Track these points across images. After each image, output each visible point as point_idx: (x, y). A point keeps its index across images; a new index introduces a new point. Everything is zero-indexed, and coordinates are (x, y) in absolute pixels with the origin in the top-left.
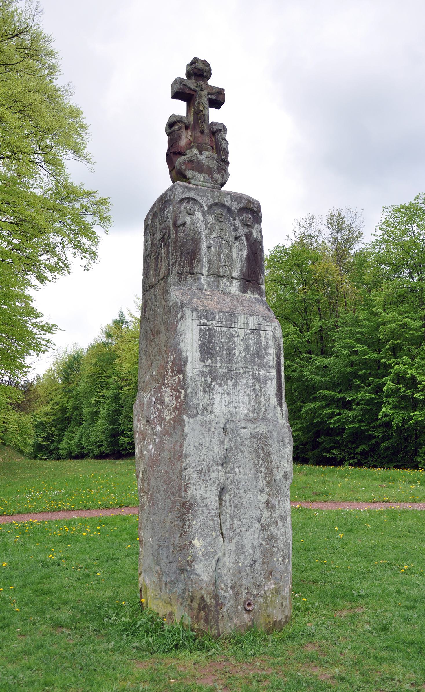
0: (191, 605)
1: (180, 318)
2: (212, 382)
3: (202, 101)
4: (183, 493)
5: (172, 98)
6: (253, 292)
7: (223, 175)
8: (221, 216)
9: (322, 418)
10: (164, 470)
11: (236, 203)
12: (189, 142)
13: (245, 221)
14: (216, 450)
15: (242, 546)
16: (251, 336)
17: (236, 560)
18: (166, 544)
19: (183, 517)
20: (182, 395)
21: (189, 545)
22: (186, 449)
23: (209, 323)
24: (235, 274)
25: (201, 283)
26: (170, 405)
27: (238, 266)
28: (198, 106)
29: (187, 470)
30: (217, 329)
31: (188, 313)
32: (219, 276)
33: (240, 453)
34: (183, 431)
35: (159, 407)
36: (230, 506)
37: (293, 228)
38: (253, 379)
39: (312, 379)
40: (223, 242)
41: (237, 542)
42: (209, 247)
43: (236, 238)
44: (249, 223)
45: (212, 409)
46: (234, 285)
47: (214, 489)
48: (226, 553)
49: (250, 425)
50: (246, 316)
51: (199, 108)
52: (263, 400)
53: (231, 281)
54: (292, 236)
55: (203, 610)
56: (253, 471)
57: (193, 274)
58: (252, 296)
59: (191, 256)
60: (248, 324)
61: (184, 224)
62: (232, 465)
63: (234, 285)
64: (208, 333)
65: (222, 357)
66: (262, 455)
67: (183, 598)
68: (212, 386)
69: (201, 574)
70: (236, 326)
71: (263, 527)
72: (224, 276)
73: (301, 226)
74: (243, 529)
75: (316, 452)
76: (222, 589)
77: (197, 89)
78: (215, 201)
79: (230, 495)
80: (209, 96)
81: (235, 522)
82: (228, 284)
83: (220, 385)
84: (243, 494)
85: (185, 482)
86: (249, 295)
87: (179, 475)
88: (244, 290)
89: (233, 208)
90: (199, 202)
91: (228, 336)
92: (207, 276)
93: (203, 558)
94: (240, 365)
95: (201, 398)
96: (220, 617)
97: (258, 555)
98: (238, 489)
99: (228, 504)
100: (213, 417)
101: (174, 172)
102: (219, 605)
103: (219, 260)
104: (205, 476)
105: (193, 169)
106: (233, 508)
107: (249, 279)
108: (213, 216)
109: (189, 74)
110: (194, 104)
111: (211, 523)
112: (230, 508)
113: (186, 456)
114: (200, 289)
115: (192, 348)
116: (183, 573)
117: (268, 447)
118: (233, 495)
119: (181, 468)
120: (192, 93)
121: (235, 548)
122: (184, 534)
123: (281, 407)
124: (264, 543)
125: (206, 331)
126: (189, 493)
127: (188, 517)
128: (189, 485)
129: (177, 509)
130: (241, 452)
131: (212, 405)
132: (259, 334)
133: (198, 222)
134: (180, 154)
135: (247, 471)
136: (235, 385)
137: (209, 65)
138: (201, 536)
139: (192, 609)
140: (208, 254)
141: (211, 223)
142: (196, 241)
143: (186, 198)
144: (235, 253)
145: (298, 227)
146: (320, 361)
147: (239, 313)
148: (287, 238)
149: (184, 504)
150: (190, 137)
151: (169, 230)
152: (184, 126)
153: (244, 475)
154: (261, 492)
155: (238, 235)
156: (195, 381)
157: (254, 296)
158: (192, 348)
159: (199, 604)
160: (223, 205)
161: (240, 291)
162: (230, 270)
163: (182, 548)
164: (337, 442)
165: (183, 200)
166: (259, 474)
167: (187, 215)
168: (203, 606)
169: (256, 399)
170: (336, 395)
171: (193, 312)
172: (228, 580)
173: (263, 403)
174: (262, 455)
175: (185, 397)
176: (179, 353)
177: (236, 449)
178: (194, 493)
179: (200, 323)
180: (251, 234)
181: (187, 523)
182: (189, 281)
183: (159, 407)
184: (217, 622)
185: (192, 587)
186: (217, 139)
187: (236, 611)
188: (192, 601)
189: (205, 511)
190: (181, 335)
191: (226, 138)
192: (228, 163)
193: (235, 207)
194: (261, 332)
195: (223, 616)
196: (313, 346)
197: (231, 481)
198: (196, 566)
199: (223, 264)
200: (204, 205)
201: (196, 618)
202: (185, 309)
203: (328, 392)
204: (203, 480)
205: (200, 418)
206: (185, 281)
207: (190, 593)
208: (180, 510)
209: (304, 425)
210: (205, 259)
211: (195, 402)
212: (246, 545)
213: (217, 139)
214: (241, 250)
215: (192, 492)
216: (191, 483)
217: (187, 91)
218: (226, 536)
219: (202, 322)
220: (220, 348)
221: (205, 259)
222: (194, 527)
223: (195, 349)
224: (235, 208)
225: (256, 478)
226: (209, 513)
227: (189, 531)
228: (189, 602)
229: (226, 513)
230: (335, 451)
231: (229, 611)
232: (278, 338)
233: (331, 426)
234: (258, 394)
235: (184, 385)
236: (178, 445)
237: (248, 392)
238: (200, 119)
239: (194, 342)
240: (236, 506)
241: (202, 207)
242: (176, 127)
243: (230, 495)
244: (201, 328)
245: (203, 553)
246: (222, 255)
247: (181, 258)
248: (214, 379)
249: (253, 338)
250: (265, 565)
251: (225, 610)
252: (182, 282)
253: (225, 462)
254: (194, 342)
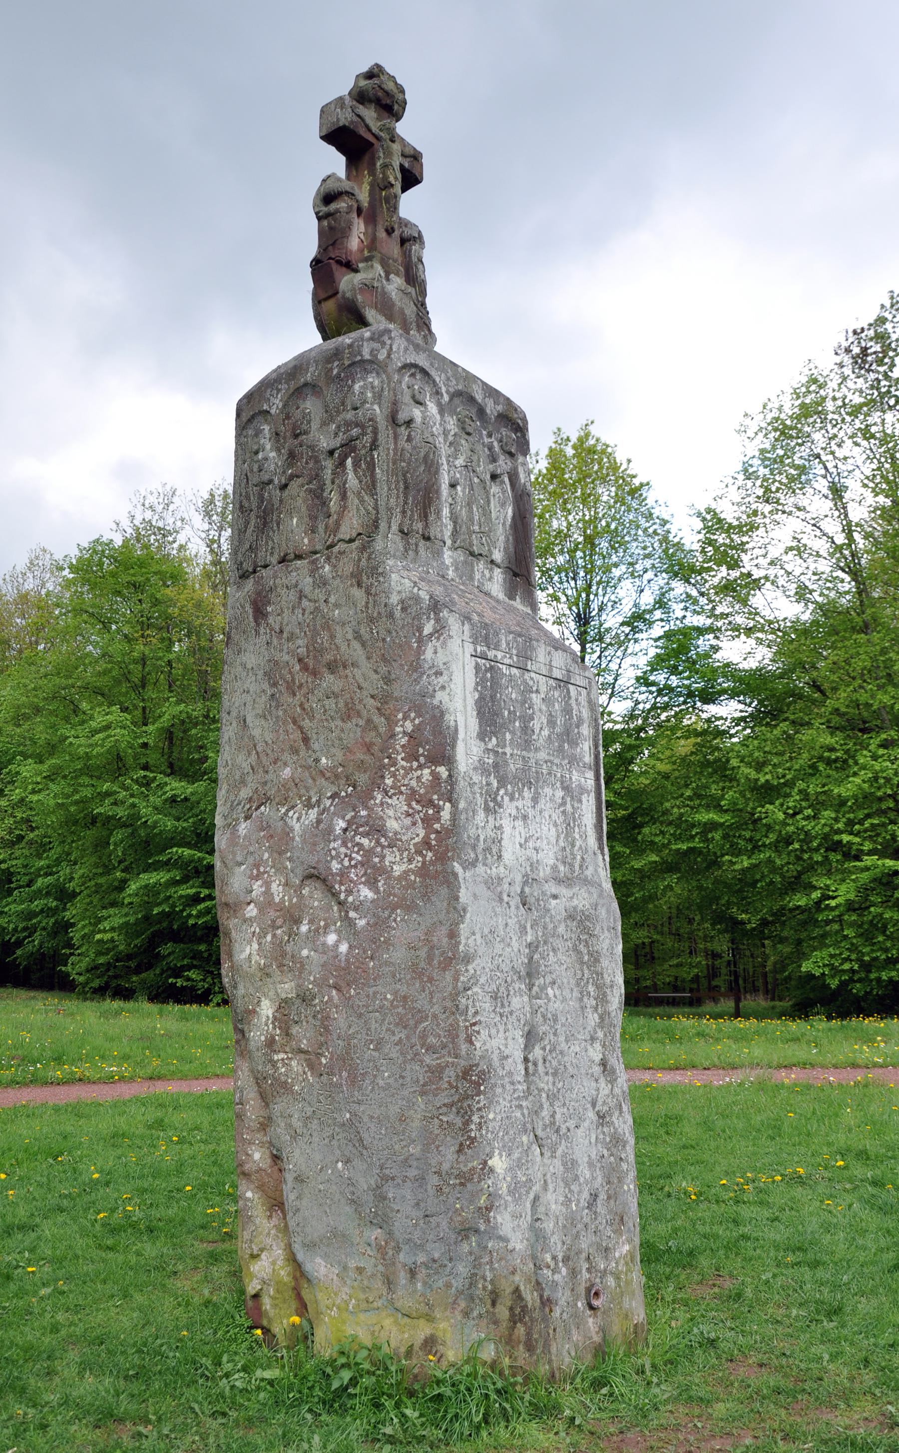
0: (494, 1314)
1: (431, 635)
2: (498, 789)
4: (464, 1047)
5: (322, 138)
9: (173, 906)
10: (395, 993)
14: (515, 944)
15: (574, 1163)
16: (557, 694)
17: (566, 1197)
18: (412, 1173)
19: (465, 1104)
20: (446, 815)
21: (482, 1169)
22: (468, 940)
23: (491, 654)
24: (498, 556)
25: (443, 563)
26: (404, 838)
29: (469, 992)
31: (453, 623)
33: (551, 953)
34: (457, 898)
35: (365, 842)
36: (547, 1074)
37: (131, 508)
38: (563, 788)
39: (156, 822)
41: (564, 1155)
42: (453, 486)
45: (500, 851)
47: (518, 1034)
48: (549, 1181)
49: (563, 891)
50: (549, 648)
51: (385, 177)
52: (577, 836)
54: (126, 524)
55: (521, 1320)
56: (576, 994)
61: (409, 423)
62: (542, 980)
64: (489, 675)
65: (513, 733)
66: (586, 958)
67: (472, 1298)
68: (499, 798)
69: (509, 1236)
70: (534, 668)
71: (601, 1116)
73: (147, 505)
74: (571, 1124)
75: (149, 976)
76: (549, 1267)
77: (382, 134)
78: (460, 387)
79: (544, 1049)
81: (557, 1110)
83: (512, 799)
84: (563, 1046)
85: (466, 1020)
87: (449, 1004)
89: (488, 411)
90: (434, 381)
93: (509, 1198)
94: (542, 755)
95: (479, 825)
96: (551, 1332)
97: (599, 1180)
98: (555, 1034)
99: (541, 1068)
100: (502, 869)
101: (330, 306)
102: (547, 1303)
104: (503, 1006)
106: (551, 1078)
107: (517, 571)
110: (375, 165)
111: (519, 1114)
112: (546, 1078)
113: (468, 959)
115: (465, 707)
116: (467, 1237)
117: (594, 940)
118: (548, 1048)
119: (455, 987)
121: (562, 1168)
122: (467, 1144)
123: (603, 855)
124: (605, 1152)
125: (486, 671)
126: (478, 1045)
127: (478, 1102)
128: (476, 1028)
129: (446, 1085)
130: (554, 950)
131: (500, 842)
132: (568, 690)
134: (349, 266)
135: (566, 993)
136: (535, 800)
138: (504, 1146)
139: (496, 1322)
142: (431, 466)
145: (140, 508)
146: (176, 786)
148: (114, 527)
149: (466, 1074)
151: (375, 432)
153: (562, 1002)
154: (593, 1039)
156: (472, 785)
157: (525, 609)
158: (465, 707)
159: (511, 1309)
160: (472, 400)
163: (465, 1179)
164: (196, 955)
165: (406, 366)
166: (585, 999)
168: (519, 1313)
169: (567, 835)
170: (204, 859)
171: (463, 625)
172: (557, 1245)
173: (578, 844)
174: (586, 958)
175: (455, 820)
176: (438, 716)
177: (545, 942)
178: (488, 1046)
179: (475, 650)
181: (475, 1119)
182: (422, 552)
183: (365, 842)
184: (547, 1346)
185: (492, 1269)
187: (575, 1315)
188: (494, 1304)
189: (508, 1087)
190: (439, 673)
193: (492, 408)
195: (555, 1330)
196: (153, 757)
197: (543, 1016)
198: (499, 1220)
200: (444, 390)
201: (507, 1343)
202: (445, 613)
203: (190, 851)
204: (501, 1016)
205: (480, 869)
206: (417, 552)
207: (487, 1284)
208: (457, 1088)
209: (132, 919)
210: (446, 512)
211: (472, 832)
212: (580, 1161)
213: (410, 256)
215: (484, 1044)
216: (480, 1022)
217: (362, 132)
218: (544, 1142)
219: (479, 650)
220: (510, 712)
221: (446, 512)
222: (491, 1125)
223: (469, 708)
225: (583, 1008)
226: (515, 1091)
227: (481, 1135)
228: (489, 1306)
229: (540, 1090)
230: (193, 974)
231: (565, 1316)
233: (191, 922)
234: (570, 821)
235: (451, 792)
236: (443, 931)
237: (555, 817)
239: (469, 696)
240: (555, 1074)
243: (544, 1049)
244: (477, 664)
245: (509, 1187)
248: (502, 782)
250: (612, 1202)
251: (558, 1314)
252: (410, 552)
253: (531, 973)
254: (469, 696)
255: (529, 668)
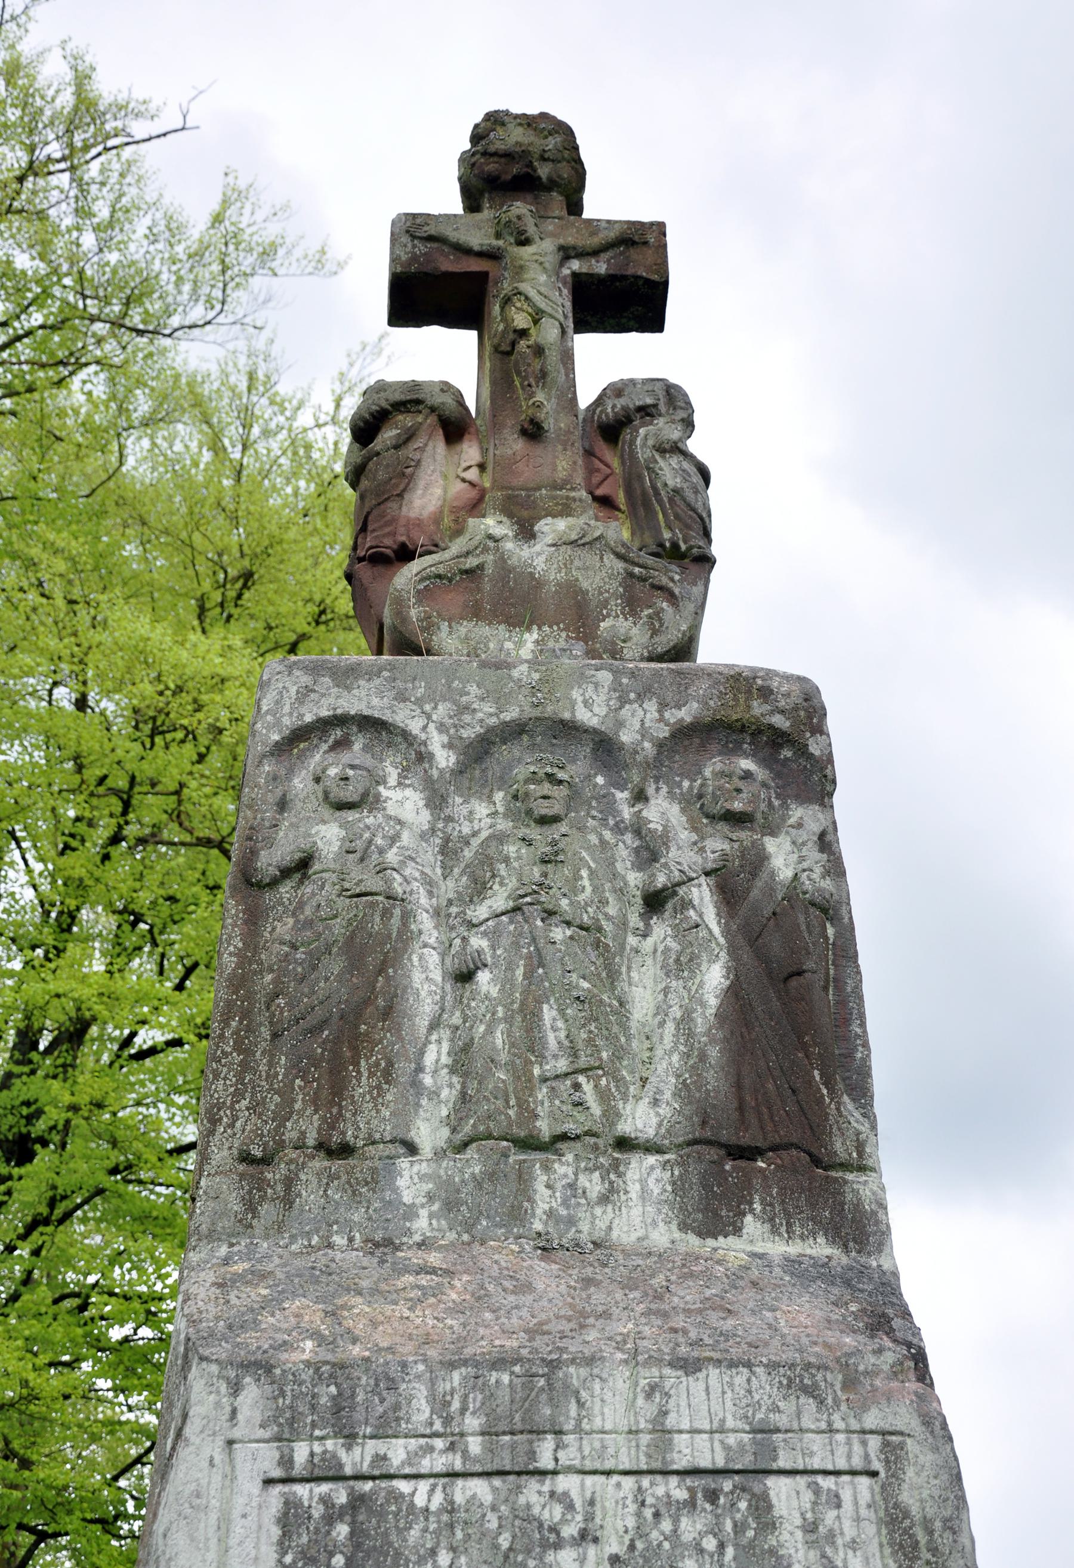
3: (524, 287)
6: (781, 1222)
7: (658, 615)
8: (546, 788)
11: (651, 706)
12: (474, 494)
13: (715, 799)
16: (690, 1527)
23: (355, 1458)
24: (641, 1119)
27: (667, 1067)
28: (504, 319)
30: (421, 1494)
32: (529, 1144)
40: (559, 933)
43: (655, 902)
44: (737, 806)
46: (634, 1189)
50: (648, 1375)
53: (616, 1165)
57: (345, 1150)
58: (778, 1248)
59: (337, 1041)
60: (662, 1433)
63: (634, 1189)
64: (342, 1530)
72: (564, 1137)
80: (575, 265)
82: (593, 1184)
86: (756, 1240)
88: (711, 1211)
89: (626, 737)
90: (405, 734)
91: (504, 1541)
92: (439, 1154)
103: (531, 1043)
105: (476, 613)
107: (746, 1139)
108: (499, 796)
109: (473, 194)
114: (388, 1242)
120: (475, 266)
125: (330, 1520)
132: (762, 1506)
133: (394, 839)
137: (565, 132)
140: (456, 1019)
141: (484, 834)
142: (373, 952)
143: (323, 725)
144: (643, 992)
147: (590, 1361)
150: (473, 474)
152: (432, 419)
155: (661, 880)
157: (794, 1249)
160: (567, 730)
161: (684, 1227)
162: (604, 1096)
165: (300, 736)
167: (326, 812)
171: (236, 1388)
179: (286, 1461)
180: (757, 861)
182: (309, 1195)
186: (629, 459)
191: (693, 445)
192: (706, 561)
194: (779, 1488)
199: (562, 1065)
206: (288, 1201)
214: (682, 965)
217: (449, 264)
219: (301, 1452)
221: (437, 1053)
224: (644, 732)
232: (927, 1524)
238: (518, 373)
241: (423, 757)
242: (388, 435)
246: (548, 1013)
247: (271, 1064)
249: (710, 1544)
252: (264, 1209)
255: (545, 1461)
